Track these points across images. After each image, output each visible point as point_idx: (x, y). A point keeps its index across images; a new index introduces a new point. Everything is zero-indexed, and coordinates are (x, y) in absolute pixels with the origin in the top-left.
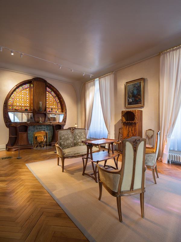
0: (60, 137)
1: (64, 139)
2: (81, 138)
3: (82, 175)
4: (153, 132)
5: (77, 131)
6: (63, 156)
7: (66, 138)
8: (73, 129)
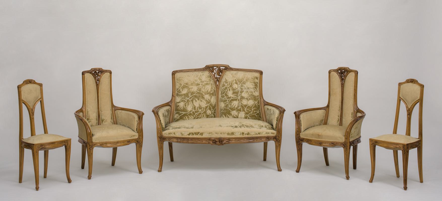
0: (178, 89)
1: (186, 95)
2: (242, 98)
3: (327, 165)
4: (38, 87)
5: (228, 76)
6: (161, 134)
7: (192, 93)
8: (220, 71)
